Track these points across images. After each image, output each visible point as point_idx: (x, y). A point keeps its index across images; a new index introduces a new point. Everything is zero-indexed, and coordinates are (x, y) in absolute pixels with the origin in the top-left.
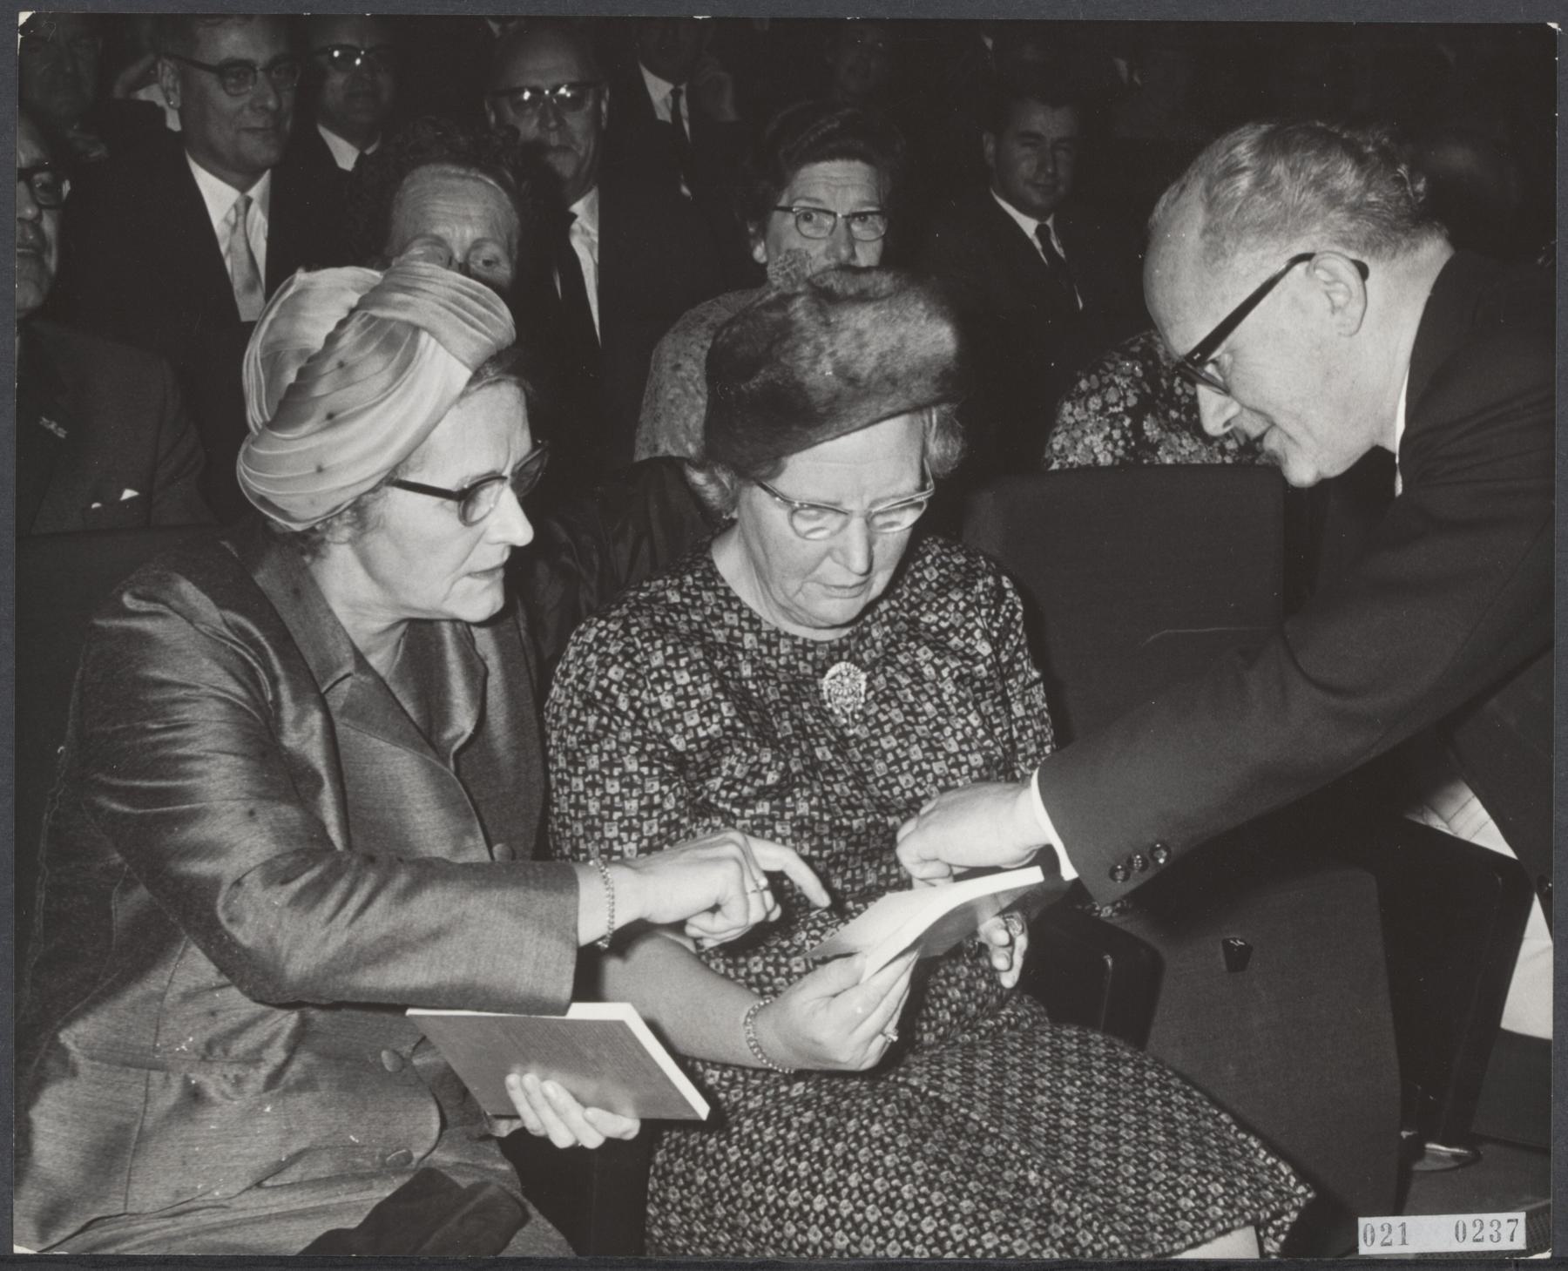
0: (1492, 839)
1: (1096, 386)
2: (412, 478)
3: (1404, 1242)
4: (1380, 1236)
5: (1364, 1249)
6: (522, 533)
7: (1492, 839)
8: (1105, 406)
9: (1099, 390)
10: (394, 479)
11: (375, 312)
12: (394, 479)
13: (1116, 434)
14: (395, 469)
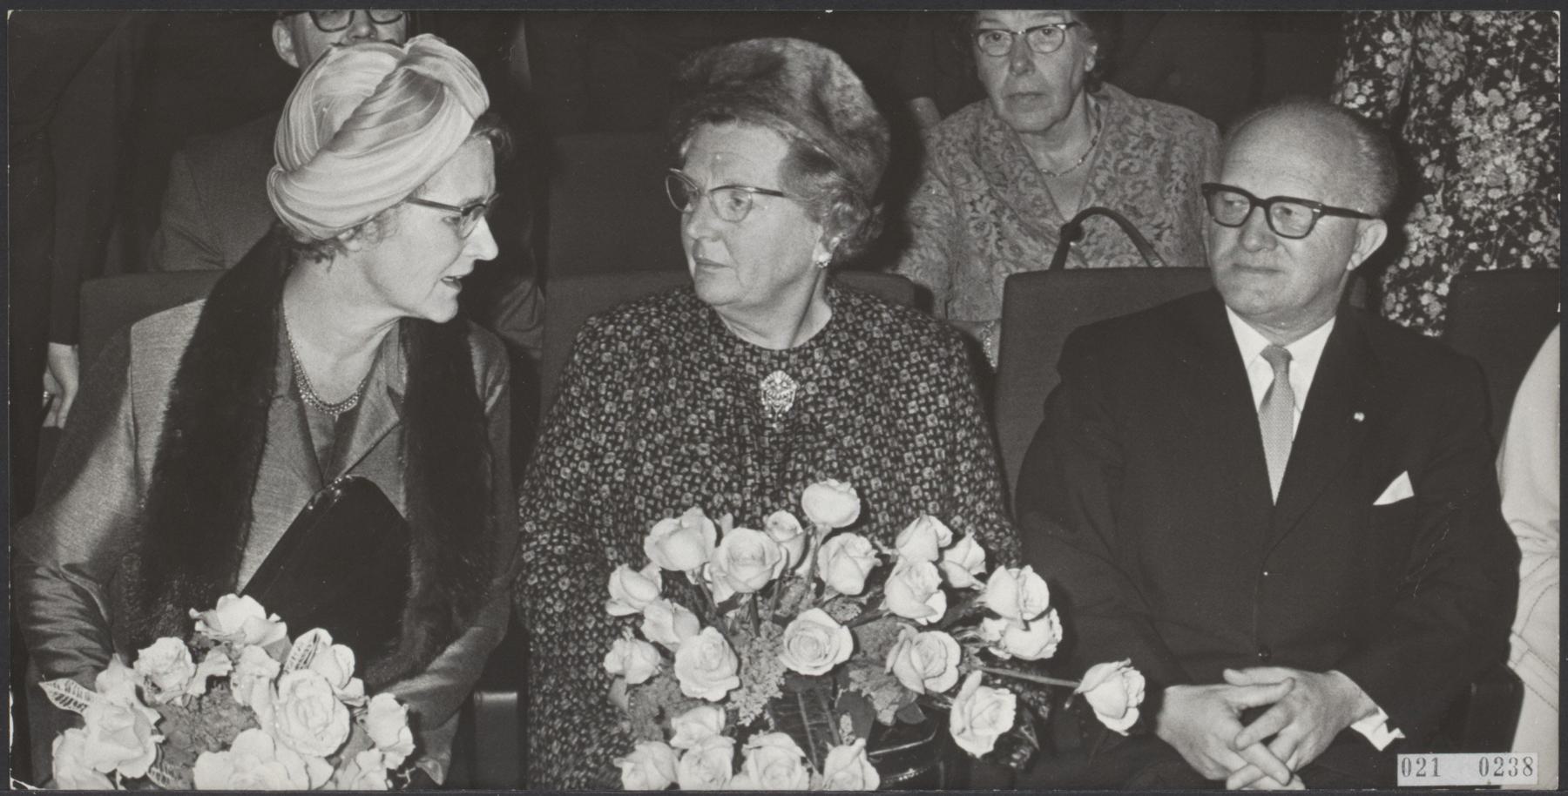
0: (1385, 499)
1: (1501, 102)
2: (428, 198)
3: (1436, 774)
4: (1416, 768)
5: (1403, 781)
6: (489, 251)
7: (1385, 499)
8: (1514, 124)
9: (1505, 108)
10: (412, 198)
11: (415, 68)
12: (412, 198)
13: (1530, 152)
14: (417, 190)
